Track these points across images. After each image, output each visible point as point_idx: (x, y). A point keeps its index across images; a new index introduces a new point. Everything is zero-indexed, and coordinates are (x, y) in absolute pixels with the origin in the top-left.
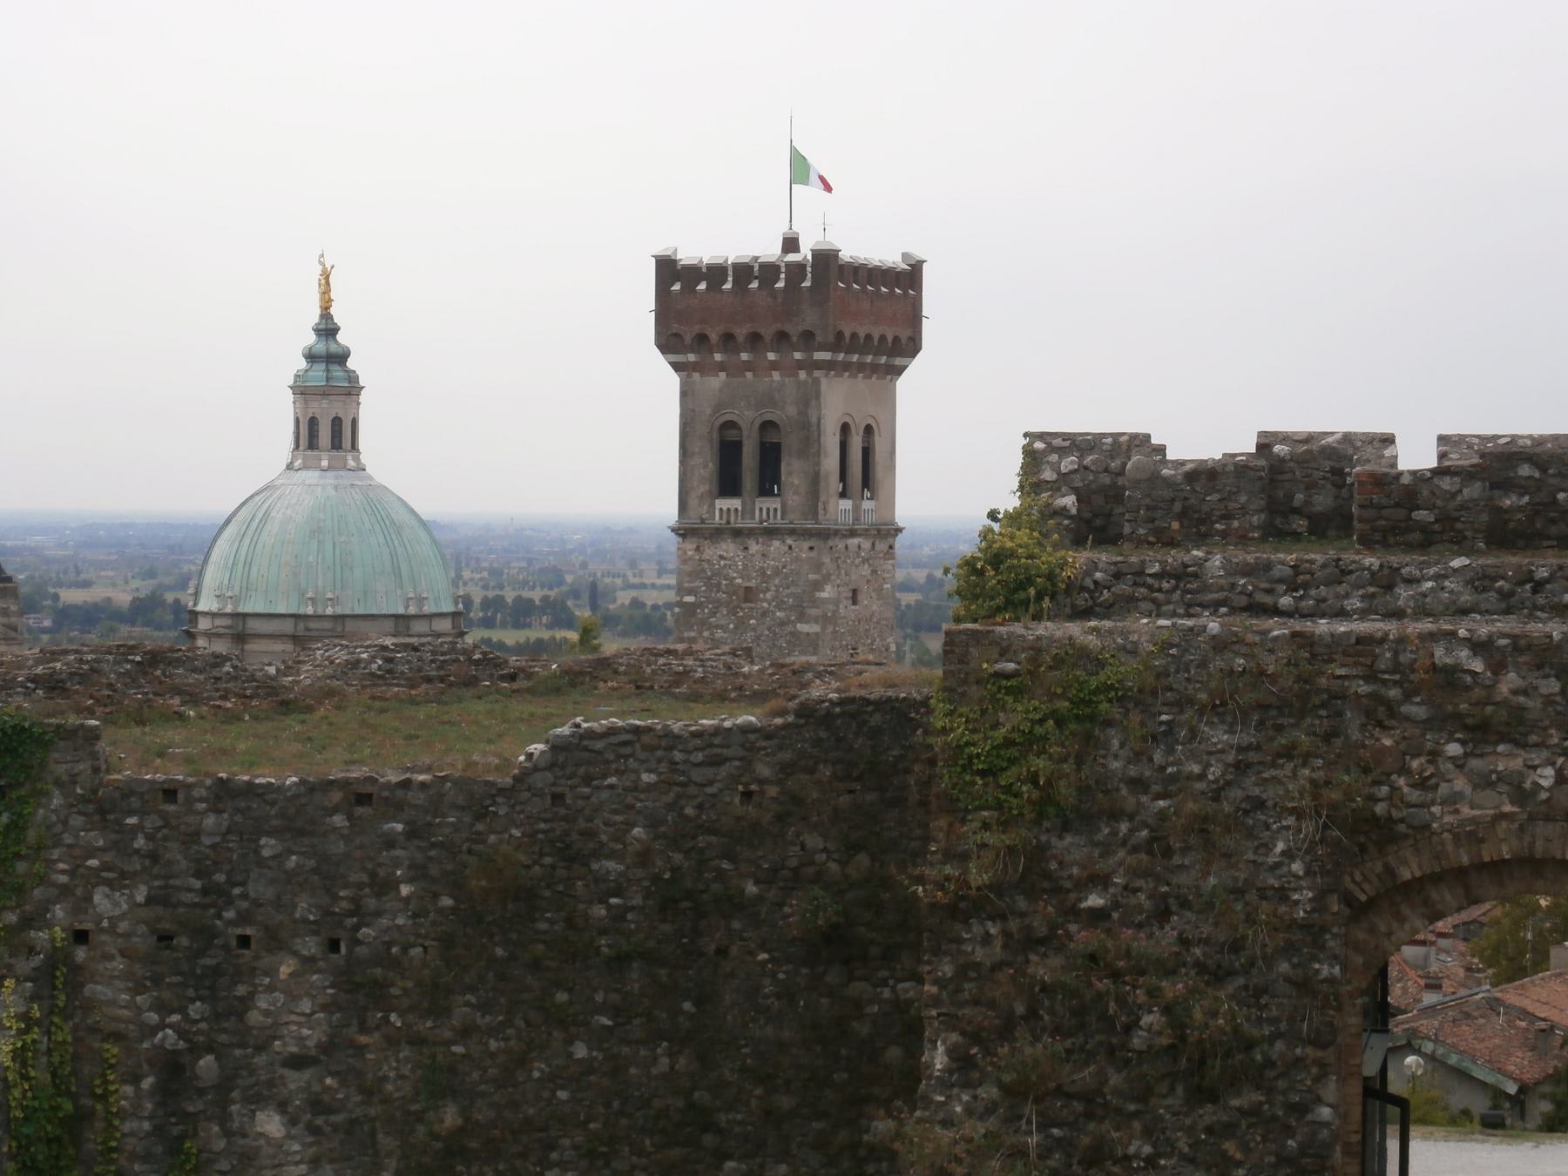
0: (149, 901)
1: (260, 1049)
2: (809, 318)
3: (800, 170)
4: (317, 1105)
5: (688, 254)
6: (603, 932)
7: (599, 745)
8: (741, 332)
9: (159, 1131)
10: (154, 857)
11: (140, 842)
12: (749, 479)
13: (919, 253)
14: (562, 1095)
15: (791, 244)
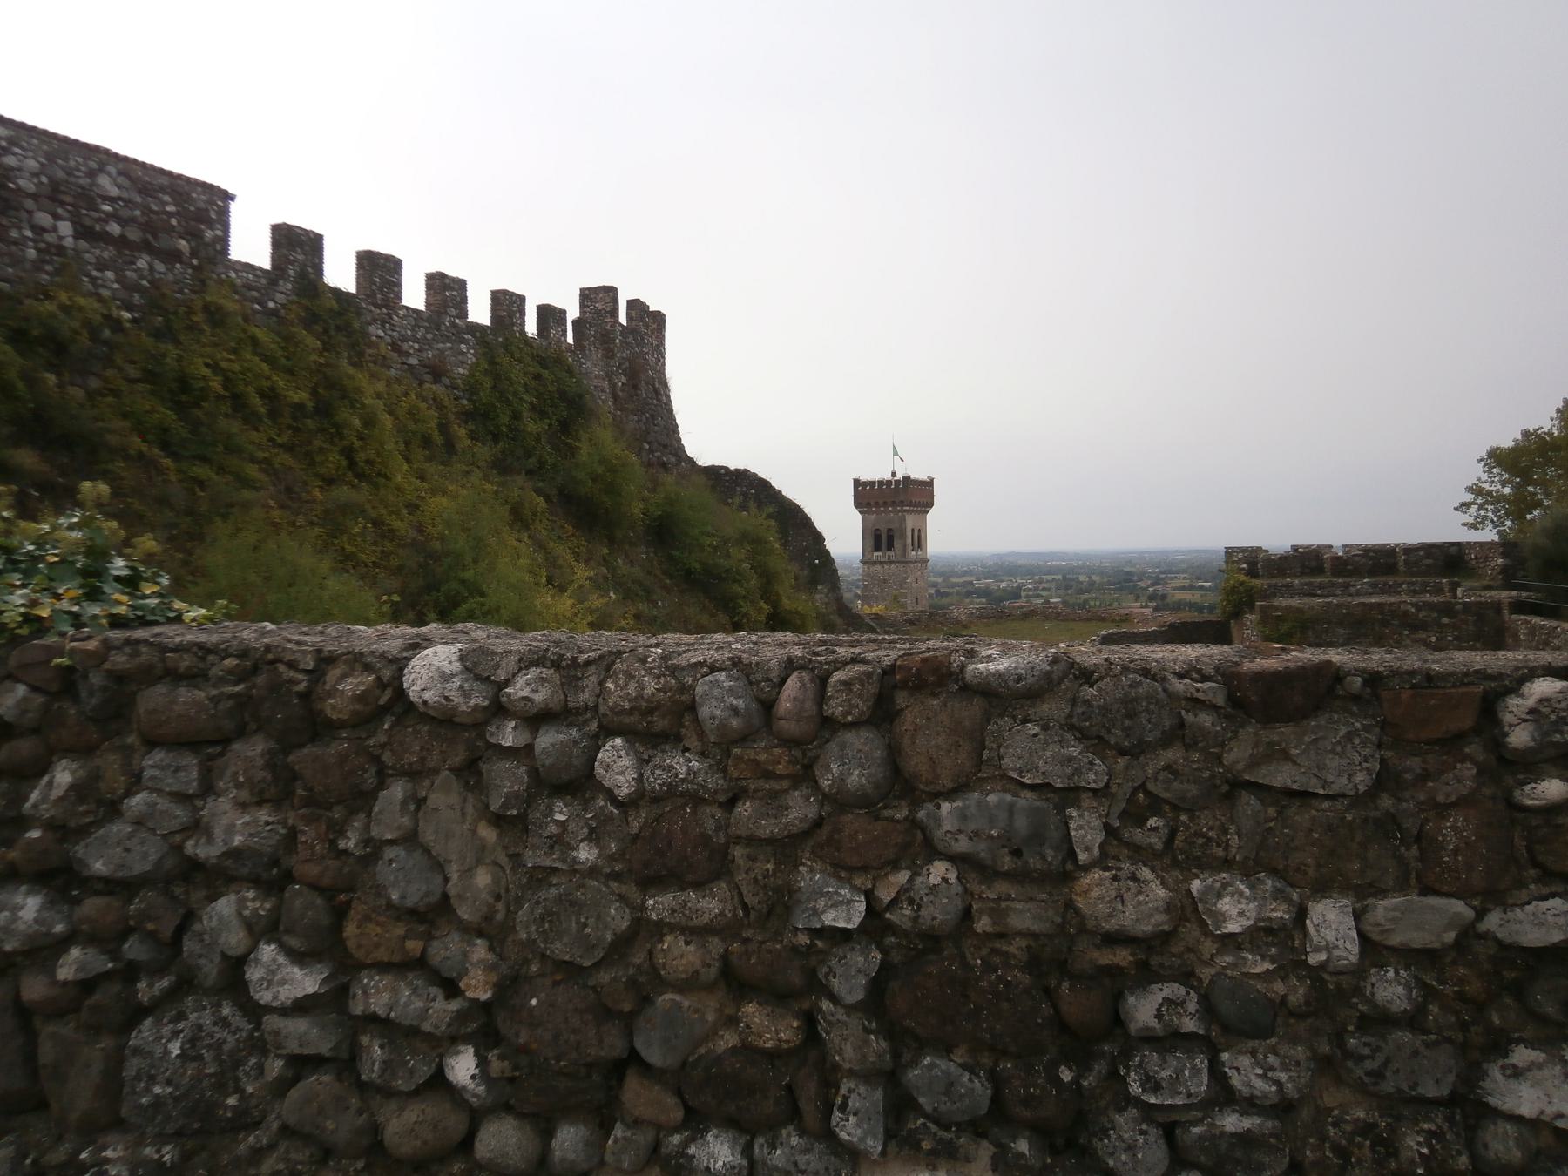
2: (902, 498)
3: (895, 453)
5: (863, 478)
12: (884, 546)
15: (894, 474)
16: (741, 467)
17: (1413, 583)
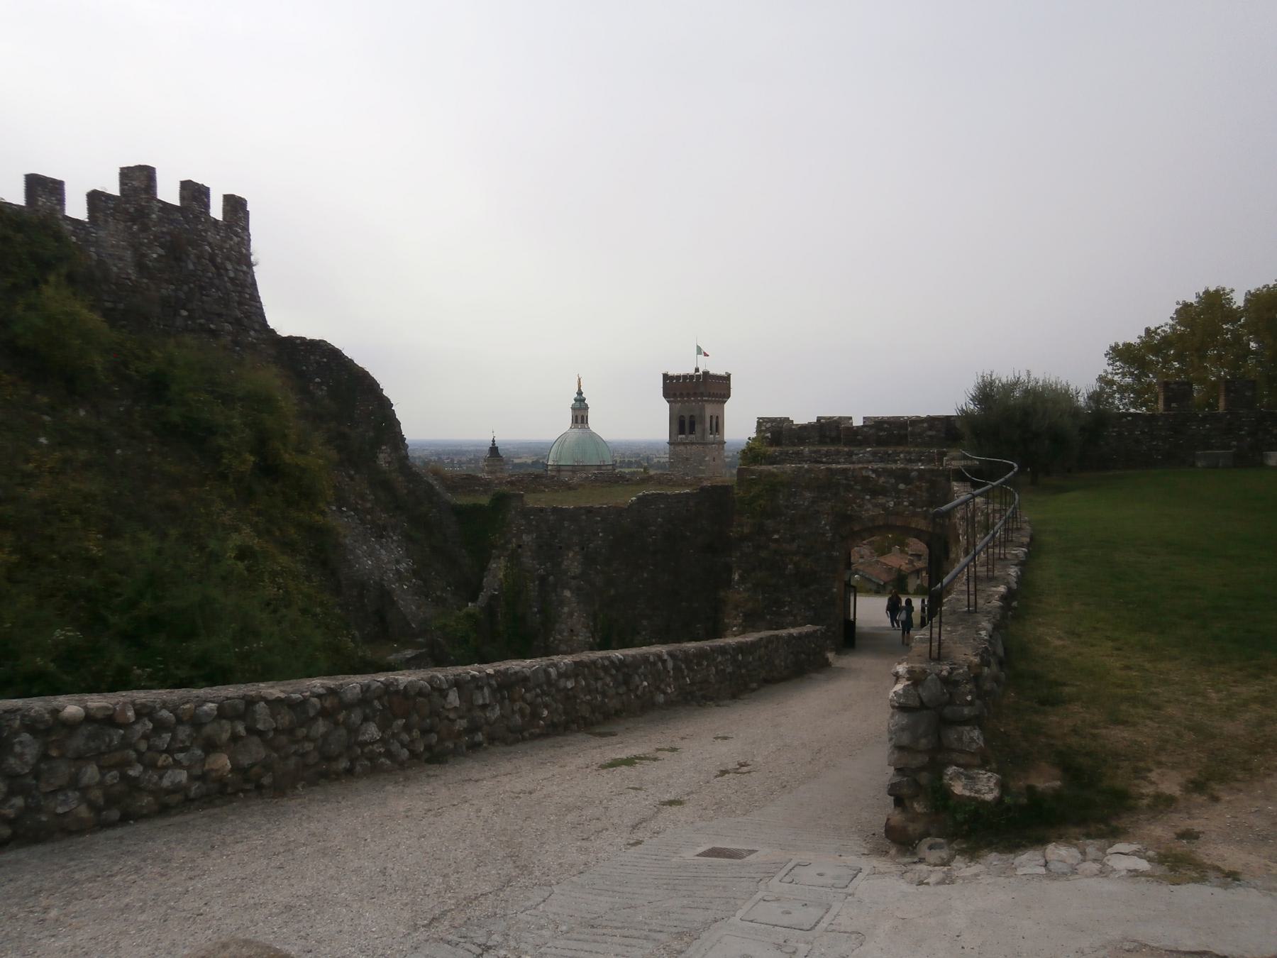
5: (671, 373)
15: (697, 370)
17: (909, 453)
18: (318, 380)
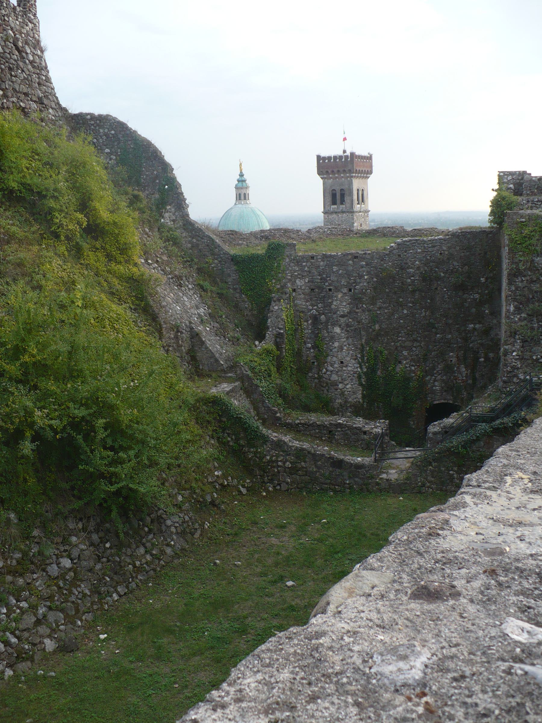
0: (309, 282)
1: (334, 313)
4: (348, 325)
5: (323, 155)
6: (410, 285)
7: (408, 243)
8: (335, 170)
9: (313, 332)
10: (310, 272)
11: (306, 269)
12: (338, 201)
13: (371, 153)
14: (402, 321)
15: (344, 152)
16: (104, 112)
18: (107, 150)
